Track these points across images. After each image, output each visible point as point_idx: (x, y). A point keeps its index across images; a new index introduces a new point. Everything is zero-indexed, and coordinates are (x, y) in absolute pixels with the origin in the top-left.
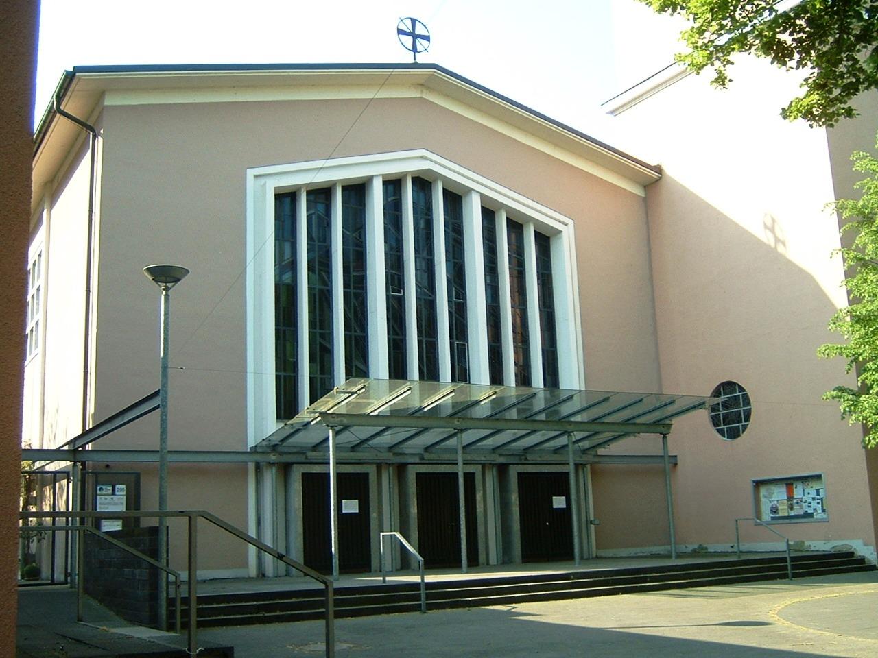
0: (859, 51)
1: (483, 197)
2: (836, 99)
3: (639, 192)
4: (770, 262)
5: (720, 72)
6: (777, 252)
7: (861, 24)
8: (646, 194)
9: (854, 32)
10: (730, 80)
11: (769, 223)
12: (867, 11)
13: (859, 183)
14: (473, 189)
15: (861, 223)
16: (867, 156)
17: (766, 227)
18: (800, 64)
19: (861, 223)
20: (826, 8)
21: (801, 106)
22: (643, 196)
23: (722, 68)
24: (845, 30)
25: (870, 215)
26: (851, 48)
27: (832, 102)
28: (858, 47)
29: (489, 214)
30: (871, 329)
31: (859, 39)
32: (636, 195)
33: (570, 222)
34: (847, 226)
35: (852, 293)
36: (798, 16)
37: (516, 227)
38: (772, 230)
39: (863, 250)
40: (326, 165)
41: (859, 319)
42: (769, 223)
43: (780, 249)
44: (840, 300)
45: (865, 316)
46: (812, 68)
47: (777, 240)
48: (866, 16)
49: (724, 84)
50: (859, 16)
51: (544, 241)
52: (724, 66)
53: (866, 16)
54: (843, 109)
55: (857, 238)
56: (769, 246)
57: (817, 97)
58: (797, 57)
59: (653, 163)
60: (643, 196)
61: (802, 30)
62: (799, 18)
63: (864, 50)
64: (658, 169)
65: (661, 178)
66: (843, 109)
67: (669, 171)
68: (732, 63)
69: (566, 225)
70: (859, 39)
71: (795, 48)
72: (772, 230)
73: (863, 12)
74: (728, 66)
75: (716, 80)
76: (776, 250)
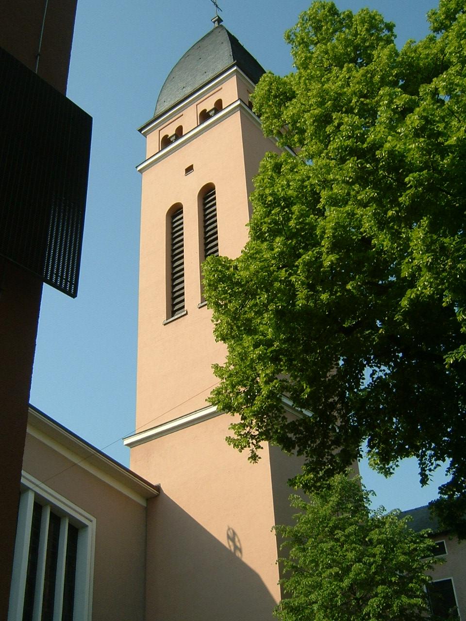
0: (333, 449)
1: (37, 496)
2: (321, 477)
3: (143, 503)
4: (225, 561)
5: (253, 452)
6: (236, 556)
7: (334, 434)
8: (147, 505)
9: (330, 438)
10: (260, 458)
11: (231, 534)
12: (338, 427)
13: (295, 515)
14: (31, 489)
15: (294, 542)
16: (299, 498)
17: (228, 537)
18: (300, 453)
19: (294, 542)
20: (316, 422)
21: (302, 480)
22: (146, 506)
23: (254, 449)
24: (326, 436)
25: (300, 537)
26: (329, 447)
27: (319, 479)
28: (332, 447)
29: (39, 505)
30: (299, 617)
31: (334, 443)
32: (139, 503)
33: (94, 520)
34: (285, 543)
35: (285, 590)
36: (300, 425)
37: (57, 517)
38: (233, 540)
39: (296, 561)
40: (34, 486)
41: (293, 609)
42: (231, 534)
43: (238, 554)
44: (276, 592)
45: (296, 607)
46: (306, 457)
47: (236, 547)
48: (338, 431)
49: (255, 460)
50: (334, 429)
51: (76, 530)
52: (256, 449)
53: (338, 431)
54: (326, 484)
55: (291, 552)
56: (230, 551)
57: (312, 476)
58: (297, 448)
59: (154, 483)
60: (146, 506)
61: (301, 433)
62: (301, 426)
63: (336, 449)
64: (158, 488)
65: (158, 495)
66: (326, 484)
67: (166, 490)
68: (262, 448)
69: (91, 521)
70: (334, 443)
71: (297, 442)
72: (233, 540)
73: (337, 429)
74: (259, 450)
75: (251, 457)
76: (235, 555)
